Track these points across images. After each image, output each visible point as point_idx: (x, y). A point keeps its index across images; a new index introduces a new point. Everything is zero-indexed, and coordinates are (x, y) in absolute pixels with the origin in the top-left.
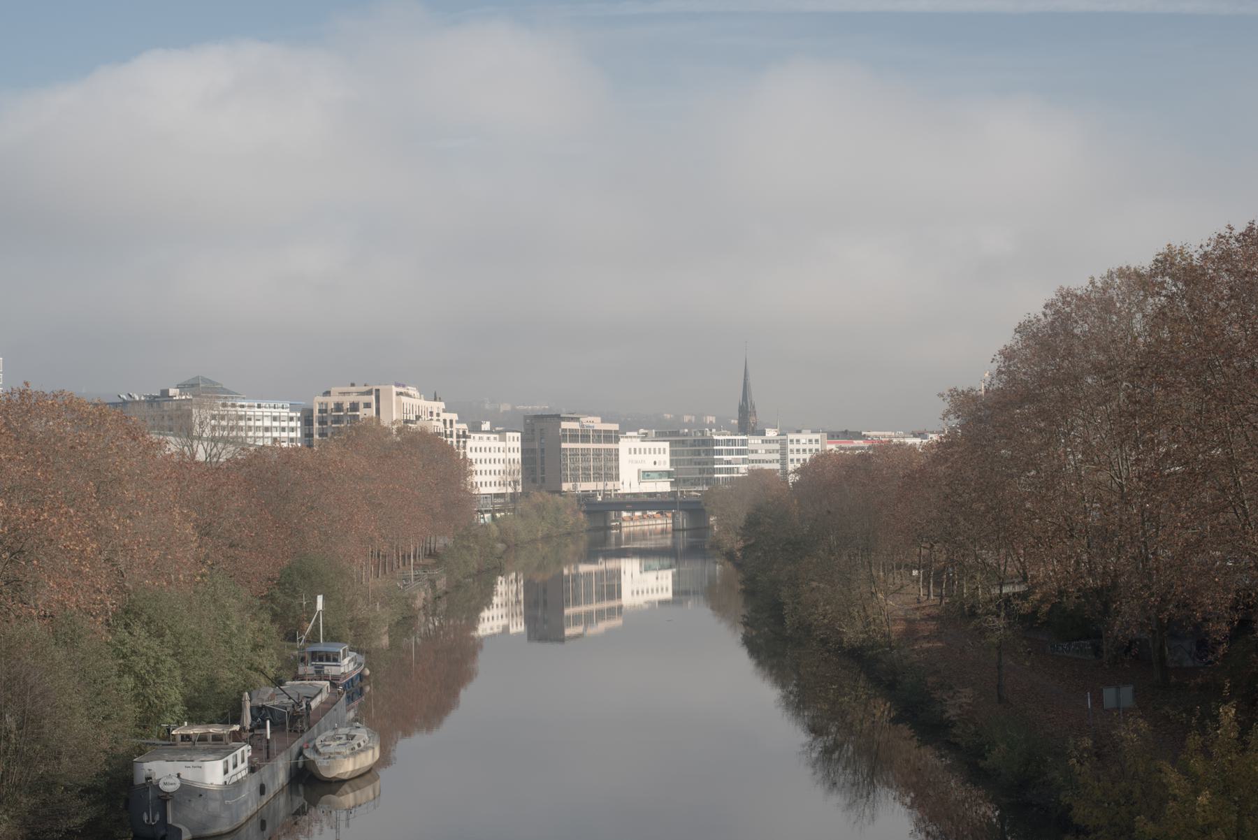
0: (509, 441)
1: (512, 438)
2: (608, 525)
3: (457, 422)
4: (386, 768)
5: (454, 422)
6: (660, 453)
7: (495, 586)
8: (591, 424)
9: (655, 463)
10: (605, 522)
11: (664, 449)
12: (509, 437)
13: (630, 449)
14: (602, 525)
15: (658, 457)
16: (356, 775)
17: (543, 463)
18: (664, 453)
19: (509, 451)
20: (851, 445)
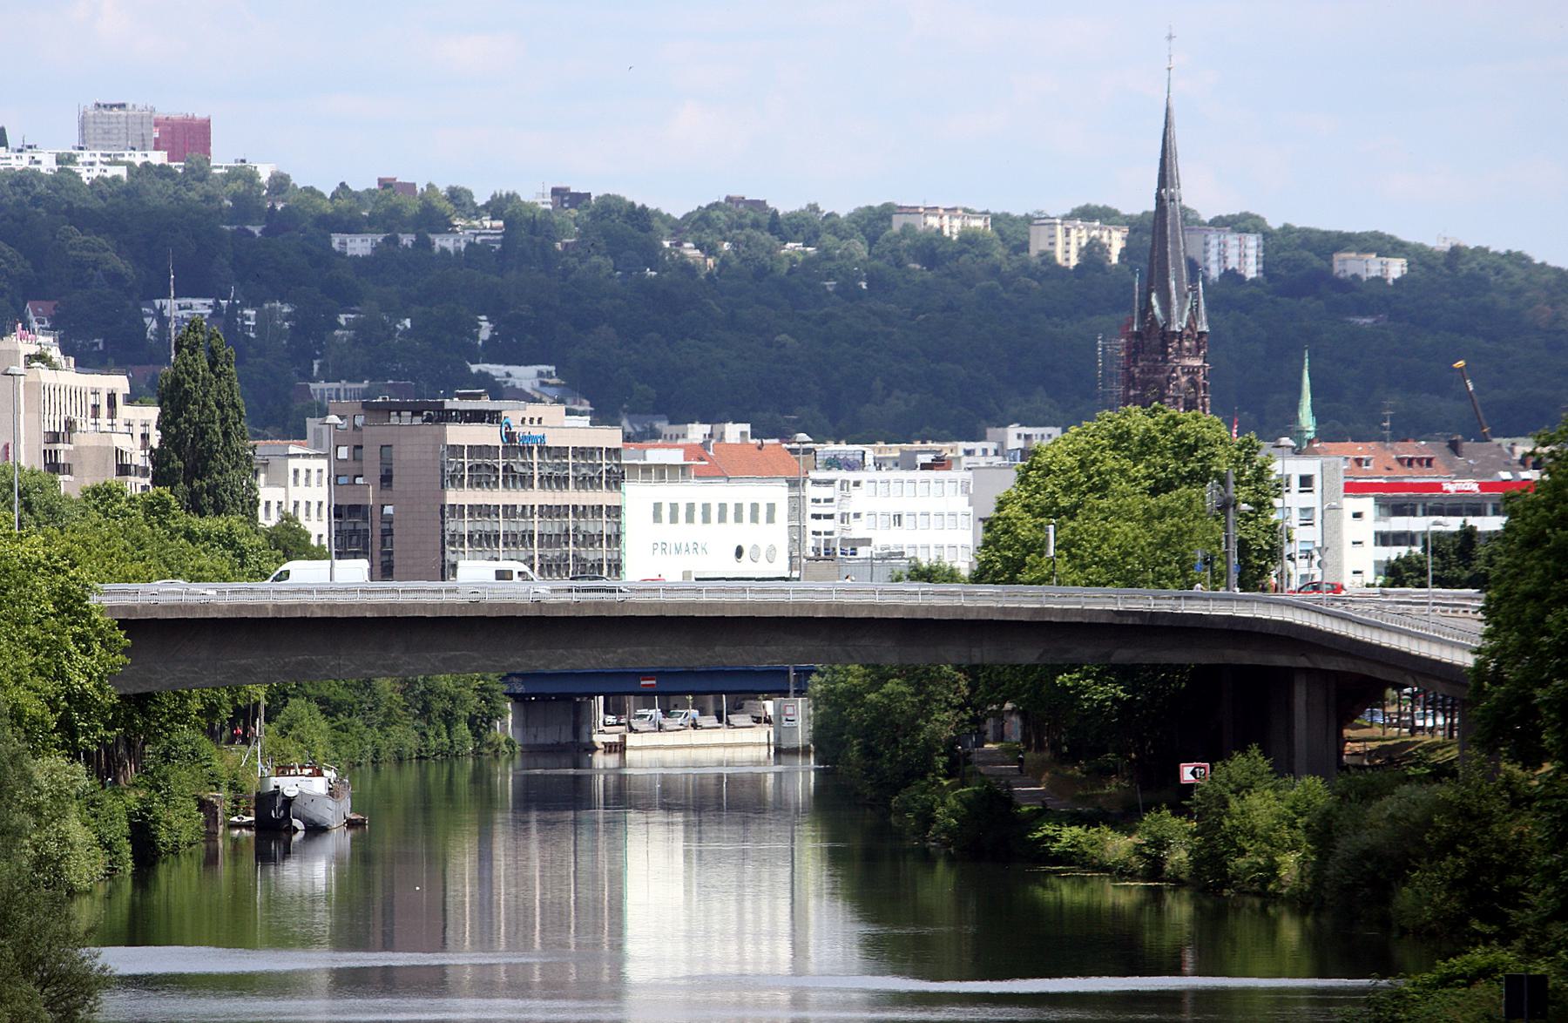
0: (296, 482)
1: (302, 475)
2: (585, 740)
3: (130, 400)
4: (1027, 215)
5: (119, 400)
6: (754, 519)
7: (41, 188)
8: (536, 431)
9: (739, 552)
10: (576, 732)
11: (771, 508)
12: (296, 472)
13: (657, 507)
14: (566, 736)
15: (746, 534)
16: (448, 869)
17: (271, 1014)
18: (770, 519)
19: (296, 482)
20: (1232, 572)
